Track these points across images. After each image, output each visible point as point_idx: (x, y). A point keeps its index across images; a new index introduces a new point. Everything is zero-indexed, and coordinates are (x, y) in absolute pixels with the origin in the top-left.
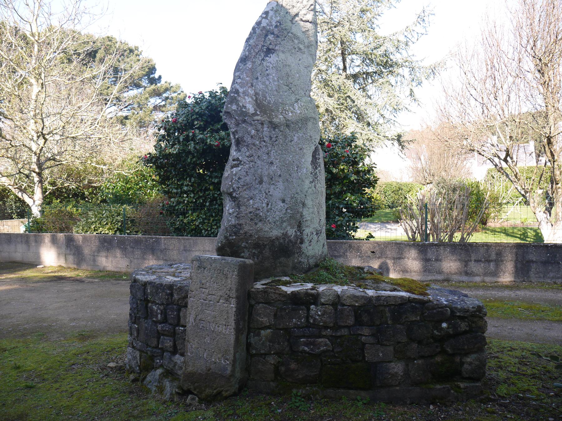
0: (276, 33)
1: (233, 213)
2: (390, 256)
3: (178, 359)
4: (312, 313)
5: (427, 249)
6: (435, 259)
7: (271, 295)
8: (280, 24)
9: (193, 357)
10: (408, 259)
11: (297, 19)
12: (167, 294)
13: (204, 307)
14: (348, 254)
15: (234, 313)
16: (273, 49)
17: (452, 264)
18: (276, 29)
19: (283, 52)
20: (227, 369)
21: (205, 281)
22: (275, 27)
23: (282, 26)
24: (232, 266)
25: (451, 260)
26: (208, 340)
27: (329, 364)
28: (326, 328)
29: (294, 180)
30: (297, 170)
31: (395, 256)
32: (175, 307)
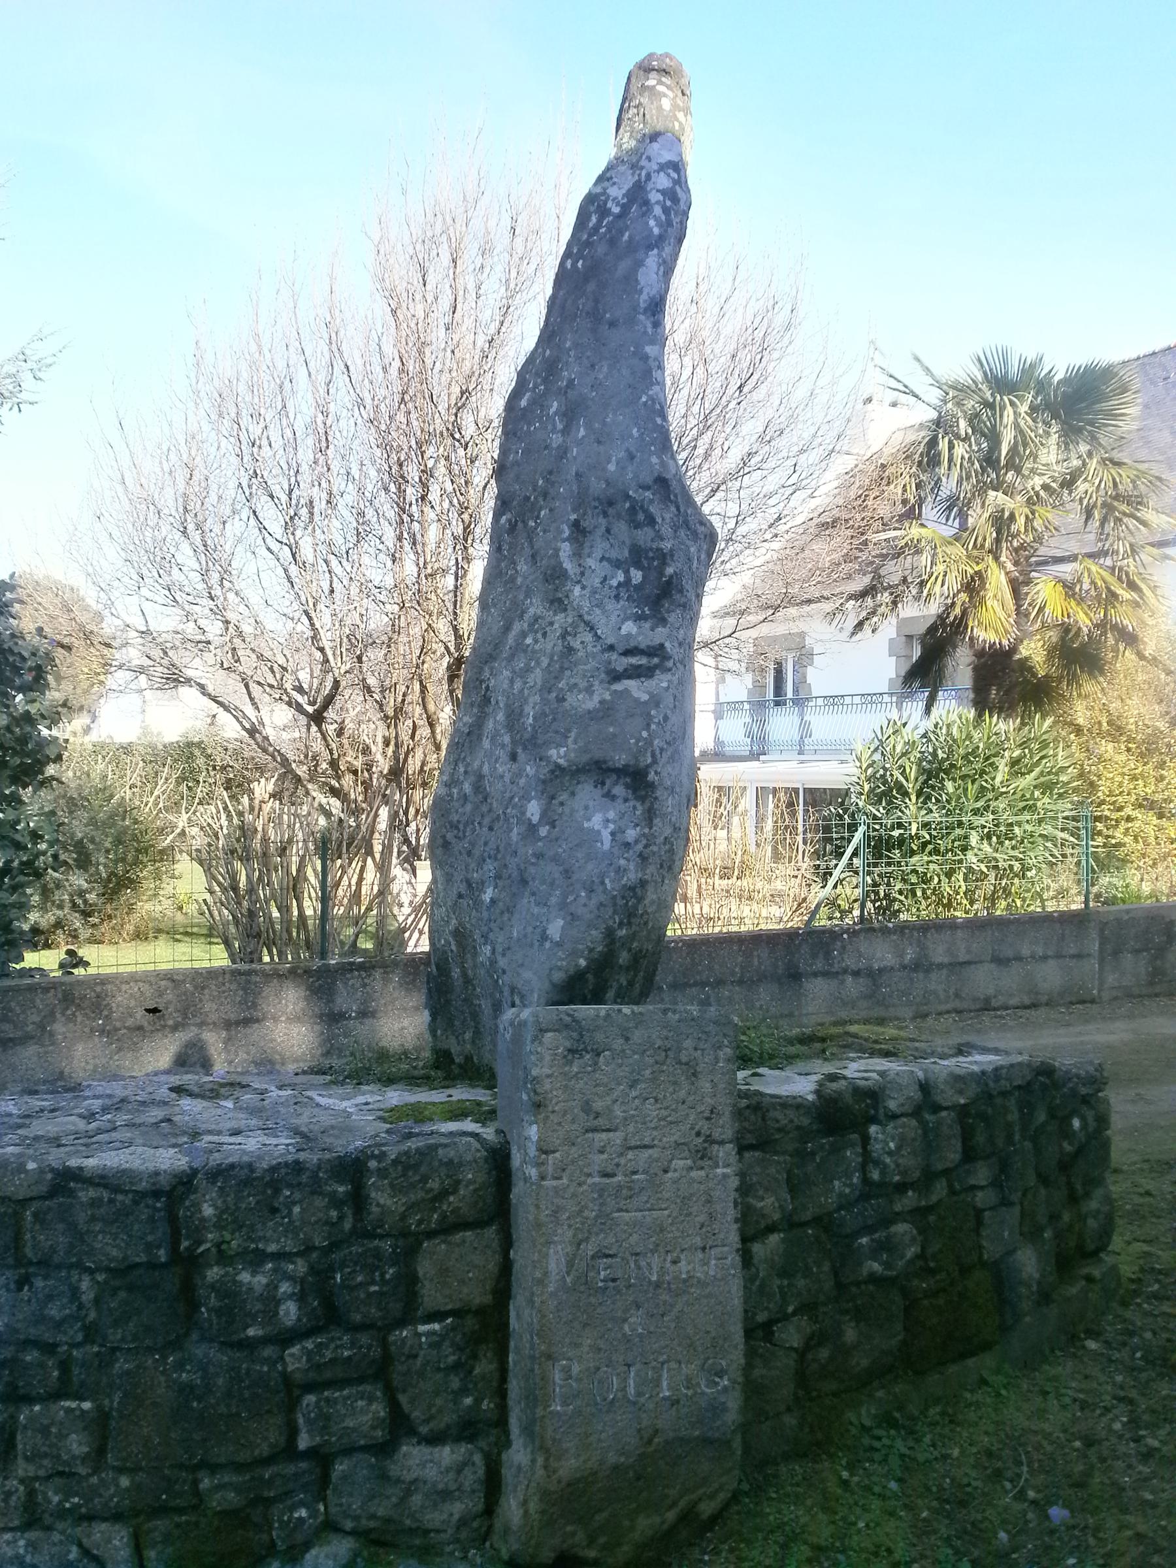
1: (637, 842)
2: (213, 1017)
3: (423, 1465)
4: (876, 1148)
6: (358, 1013)
7: (772, 1114)
10: (275, 1019)
12: (336, 1202)
14: (59, 1027)
17: (406, 1023)
20: (725, 1409)
21: (608, 1100)
24: (711, 1028)
25: (405, 1009)
26: (636, 1322)
28: (901, 1188)
32: (386, 1246)
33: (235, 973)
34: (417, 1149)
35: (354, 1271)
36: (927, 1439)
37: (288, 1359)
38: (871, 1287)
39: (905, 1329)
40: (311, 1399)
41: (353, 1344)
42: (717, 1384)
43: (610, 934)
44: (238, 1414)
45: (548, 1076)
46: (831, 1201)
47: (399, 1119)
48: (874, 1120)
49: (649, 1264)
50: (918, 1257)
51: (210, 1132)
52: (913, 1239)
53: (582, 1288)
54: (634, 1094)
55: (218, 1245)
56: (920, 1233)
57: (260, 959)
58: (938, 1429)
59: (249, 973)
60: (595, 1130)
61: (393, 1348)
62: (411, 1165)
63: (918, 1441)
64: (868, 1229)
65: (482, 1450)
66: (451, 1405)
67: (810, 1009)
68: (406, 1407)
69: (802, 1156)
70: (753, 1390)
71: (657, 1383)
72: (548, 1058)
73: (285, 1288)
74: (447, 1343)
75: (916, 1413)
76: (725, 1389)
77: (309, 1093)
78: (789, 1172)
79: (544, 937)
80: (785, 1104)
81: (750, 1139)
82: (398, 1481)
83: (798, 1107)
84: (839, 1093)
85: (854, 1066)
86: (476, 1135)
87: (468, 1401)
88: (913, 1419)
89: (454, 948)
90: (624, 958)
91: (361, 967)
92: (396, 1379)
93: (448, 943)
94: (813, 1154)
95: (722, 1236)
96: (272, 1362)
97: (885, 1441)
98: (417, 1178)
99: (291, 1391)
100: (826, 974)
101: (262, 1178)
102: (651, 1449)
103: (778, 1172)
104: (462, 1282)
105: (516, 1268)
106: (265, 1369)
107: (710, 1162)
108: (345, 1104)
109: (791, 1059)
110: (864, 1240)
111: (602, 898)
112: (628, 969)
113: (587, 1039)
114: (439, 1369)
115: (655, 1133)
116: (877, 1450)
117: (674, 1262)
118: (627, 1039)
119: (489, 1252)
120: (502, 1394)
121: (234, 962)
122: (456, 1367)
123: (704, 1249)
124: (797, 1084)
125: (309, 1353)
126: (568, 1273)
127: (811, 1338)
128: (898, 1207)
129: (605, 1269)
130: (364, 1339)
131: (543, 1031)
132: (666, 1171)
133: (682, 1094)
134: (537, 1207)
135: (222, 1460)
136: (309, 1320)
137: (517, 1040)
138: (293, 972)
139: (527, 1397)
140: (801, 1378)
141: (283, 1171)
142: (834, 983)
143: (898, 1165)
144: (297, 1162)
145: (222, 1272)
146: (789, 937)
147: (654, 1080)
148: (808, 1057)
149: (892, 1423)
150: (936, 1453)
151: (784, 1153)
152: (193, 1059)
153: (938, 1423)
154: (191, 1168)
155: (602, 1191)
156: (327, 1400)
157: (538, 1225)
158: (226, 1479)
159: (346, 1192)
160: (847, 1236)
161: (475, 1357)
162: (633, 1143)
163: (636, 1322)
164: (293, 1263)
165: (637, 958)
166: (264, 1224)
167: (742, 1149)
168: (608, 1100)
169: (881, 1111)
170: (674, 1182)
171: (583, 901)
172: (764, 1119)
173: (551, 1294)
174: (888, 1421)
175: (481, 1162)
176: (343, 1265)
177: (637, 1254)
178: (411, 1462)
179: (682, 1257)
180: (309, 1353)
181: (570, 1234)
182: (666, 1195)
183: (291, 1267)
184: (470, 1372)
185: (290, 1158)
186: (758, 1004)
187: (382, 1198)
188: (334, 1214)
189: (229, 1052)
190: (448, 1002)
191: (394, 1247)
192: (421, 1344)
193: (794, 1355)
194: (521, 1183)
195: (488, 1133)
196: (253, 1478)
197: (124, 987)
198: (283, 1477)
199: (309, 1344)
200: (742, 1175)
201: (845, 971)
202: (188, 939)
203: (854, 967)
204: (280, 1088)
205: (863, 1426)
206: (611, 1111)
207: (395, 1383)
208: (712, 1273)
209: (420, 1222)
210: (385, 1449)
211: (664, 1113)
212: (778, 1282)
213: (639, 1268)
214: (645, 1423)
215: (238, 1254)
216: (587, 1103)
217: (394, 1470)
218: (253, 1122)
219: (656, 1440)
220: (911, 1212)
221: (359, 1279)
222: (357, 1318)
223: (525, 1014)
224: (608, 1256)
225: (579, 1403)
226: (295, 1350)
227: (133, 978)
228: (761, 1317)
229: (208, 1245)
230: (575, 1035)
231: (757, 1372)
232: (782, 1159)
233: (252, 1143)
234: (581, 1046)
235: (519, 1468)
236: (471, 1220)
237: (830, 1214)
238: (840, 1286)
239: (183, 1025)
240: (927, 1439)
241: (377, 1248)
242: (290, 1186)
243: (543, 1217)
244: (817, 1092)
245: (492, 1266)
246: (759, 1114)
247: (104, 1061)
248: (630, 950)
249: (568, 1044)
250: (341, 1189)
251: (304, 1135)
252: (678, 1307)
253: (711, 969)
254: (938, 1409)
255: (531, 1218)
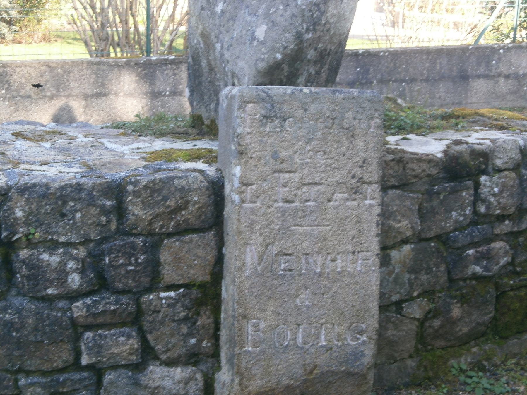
4: (484, 191)
5: (154, 72)
7: (410, 165)
9: (263, 352)
13: (290, 220)
15: (376, 218)
20: (363, 355)
21: (290, 152)
24: (367, 104)
26: (304, 298)
27: (512, 290)
28: (501, 218)
31: (89, 92)
32: (139, 241)
33: (90, 63)
34: (161, 180)
35: (117, 257)
36: (504, 379)
37: (74, 309)
38: (474, 282)
39: (496, 309)
40: (89, 334)
41: (117, 302)
42: (358, 339)
43: (299, 36)
44: (42, 341)
45: (249, 134)
46: (449, 225)
47: (155, 159)
48: (484, 172)
49: (315, 261)
50: (508, 264)
51: (27, 163)
52: (506, 253)
53: (269, 274)
54: (309, 148)
55: (27, 236)
56: (511, 249)
57: (109, 55)
58: (512, 374)
59: (99, 63)
60: (280, 171)
61: (144, 306)
62: (155, 190)
63: (497, 380)
64: (473, 245)
65: (202, 371)
66: (182, 343)
67: (474, 100)
68: (152, 343)
69: (430, 194)
70: (383, 342)
71: (317, 336)
72: (249, 121)
73: (71, 265)
74: (179, 305)
75: (499, 363)
76: (364, 342)
77: (101, 140)
78: (420, 205)
79: (253, 38)
80: (419, 159)
81: (393, 182)
82: (146, 387)
83: (430, 161)
84: (460, 153)
85: (475, 135)
86: (201, 172)
87: (193, 341)
88: (496, 366)
89: (202, 45)
90: (311, 54)
91: (172, 62)
92: (146, 326)
93: (199, 42)
94: (438, 193)
95: (367, 245)
96: (65, 312)
97: (475, 379)
98: (160, 198)
99: (77, 329)
100: (486, 77)
101: (55, 194)
102: (311, 377)
103: (412, 204)
104: (190, 266)
105: (226, 260)
106: (59, 314)
107: (360, 196)
108: (125, 148)
109: (432, 129)
110: (471, 252)
111: (294, 11)
112: (315, 62)
113: (277, 109)
114: (174, 321)
115: (323, 175)
116: (469, 384)
117: (333, 261)
118: (306, 110)
119: (209, 249)
120: (216, 337)
121: (91, 56)
122: (186, 319)
123: (354, 253)
124: (431, 146)
125: (88, 307)
126: (259, 264)
127: (429, 311)
128: (497, 231)
129: (285, 263)
130: (124, 299)
131: (246, 102)
132: (329, 201)
133: (343, 149)
134: (239, 220)
135: (33, 368)
136: (88, 286)
137: (230, 107)
138: (127, 64)
139: (230, 341)
140: (421, 337)
141: (69, 190)
142: (491, 83)
143: (499, 203)
144: (78, 184)
145: (30, 253)
146: (464, 49)
147: (323, 139)
148: (445, 128)
149: (483, 369)
150: (508, 389)
151: (417, 192)
152: (65, 118)
153: (512, 370)
154: (7, 185)
155: (284, 212)
156: (100, 336)
157: (240, 233)
158: (35, 380)
159: (112, 206)
160: (458, 248)
161: (198, 314)
162: (307, 181)
163: (304, 298)
164: (77, 249)
165: (322, 56)
166: (57, 223)
167: (385, 189)
168: (290, 152)
169: (490, 167)
170: (335, 208)
171: (281, 12)
172: (404, 169)
173: (247, 277)
174: (478, 366)
175: (204, 190)
176: (110, 252)
177: (307, 254)
178: (155, 376)
179: (339, 257)
180: (88, 307)
181: (261, 239)
182: (329, 217)
183: (76, 252)
184: (195, 323)
185: (74, 182)
186: (437, 96)
187: (136, 211)
188: (104, 219)
189: (87, 114)
190: (200, 83)
191: (145, 242)
192: (162, 304)
193: (416, 323)
194: (230, 205)
195: (211, 171)
196: (52, 381)
197: (18, 70)
198: (72, 380)
199: (88, 301)
200: (382, 204)
201: (499, 75)
202: (75, 42)
203: (505, 72)
204: (86, 136)
205: (461, 369)
206: (293, 159)
207: (145, 328)
208: (359, 269)
209: (162, 227)
210: (138, 367)
211: (330, 161)
212: (408, 276)
213: (308, 263)
214: (308, 361)
215: (40, 242)
216: (276, 152)
217: (144, 380)
218: (60, 157)
219: (315, 372)
220: (506, 234)
221: (121, 261)
222: (120, 286)
223: (235, 90)
224: (286, 255)
225: (264, 346)
226: (79, 304)
227: (23, 64)
228: (395, 298)
229: (20, 235)
230: (268, 106)
231: (389, 333)
232: (415, 196)
233: (52, 171)
234: (273, 114)
235: (224, 384)
236: (196, 227)
237: (448, 233)
238: (451, 280)
239: (57, 96)
240: (504, 379)
241: (132, 242)
242: (73, 200)
243: (243, 228)
244: (445, 152)
245: (211, 257)
246: (401, 165)
247: (7, 117)
248: (316, 49)
249: (263, 112)
250: (109, 203)
251: (89, 168)
252: (334, 289)
253: (407, 71)
254: (514, 361)
255: (235, 228)
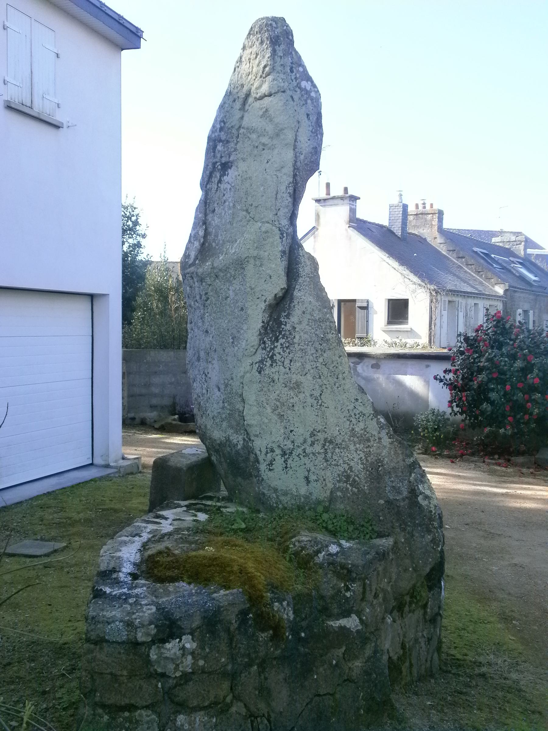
0: (223, 137)
8: (224, 124)
11: (250, 100)
16: (228, 162)
18: (223, 133)
19: (244, 160)
22: (220, 131)
23: (227, 125)
29: (229, 358)
30: (233, 343)
